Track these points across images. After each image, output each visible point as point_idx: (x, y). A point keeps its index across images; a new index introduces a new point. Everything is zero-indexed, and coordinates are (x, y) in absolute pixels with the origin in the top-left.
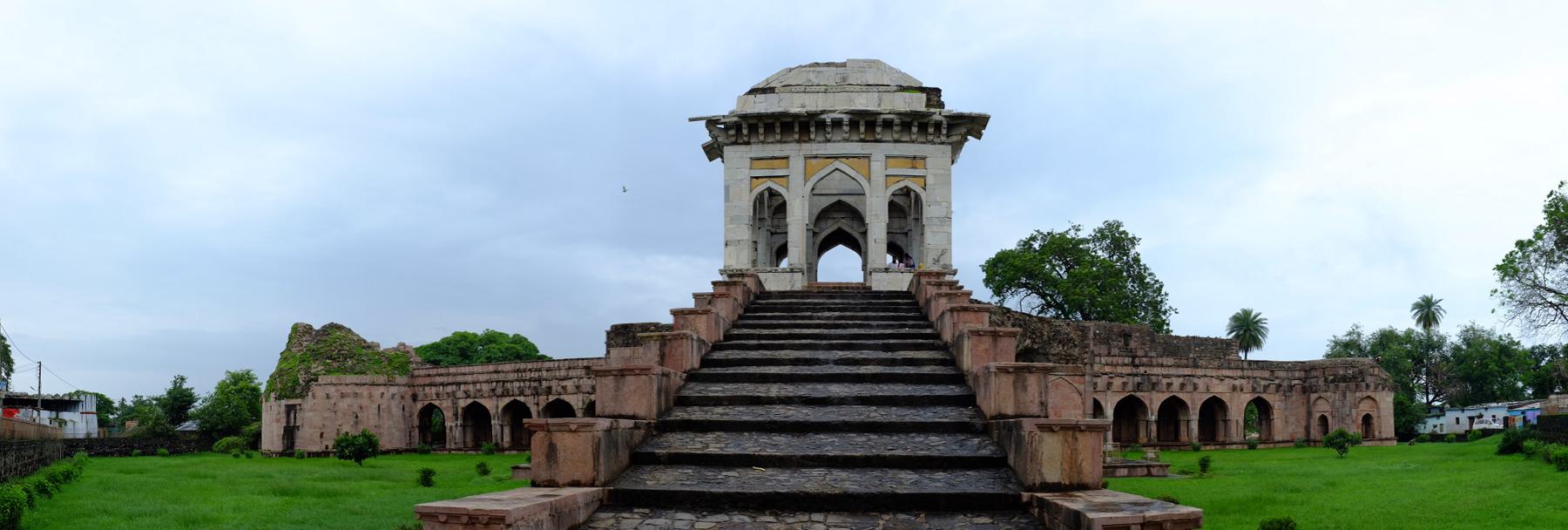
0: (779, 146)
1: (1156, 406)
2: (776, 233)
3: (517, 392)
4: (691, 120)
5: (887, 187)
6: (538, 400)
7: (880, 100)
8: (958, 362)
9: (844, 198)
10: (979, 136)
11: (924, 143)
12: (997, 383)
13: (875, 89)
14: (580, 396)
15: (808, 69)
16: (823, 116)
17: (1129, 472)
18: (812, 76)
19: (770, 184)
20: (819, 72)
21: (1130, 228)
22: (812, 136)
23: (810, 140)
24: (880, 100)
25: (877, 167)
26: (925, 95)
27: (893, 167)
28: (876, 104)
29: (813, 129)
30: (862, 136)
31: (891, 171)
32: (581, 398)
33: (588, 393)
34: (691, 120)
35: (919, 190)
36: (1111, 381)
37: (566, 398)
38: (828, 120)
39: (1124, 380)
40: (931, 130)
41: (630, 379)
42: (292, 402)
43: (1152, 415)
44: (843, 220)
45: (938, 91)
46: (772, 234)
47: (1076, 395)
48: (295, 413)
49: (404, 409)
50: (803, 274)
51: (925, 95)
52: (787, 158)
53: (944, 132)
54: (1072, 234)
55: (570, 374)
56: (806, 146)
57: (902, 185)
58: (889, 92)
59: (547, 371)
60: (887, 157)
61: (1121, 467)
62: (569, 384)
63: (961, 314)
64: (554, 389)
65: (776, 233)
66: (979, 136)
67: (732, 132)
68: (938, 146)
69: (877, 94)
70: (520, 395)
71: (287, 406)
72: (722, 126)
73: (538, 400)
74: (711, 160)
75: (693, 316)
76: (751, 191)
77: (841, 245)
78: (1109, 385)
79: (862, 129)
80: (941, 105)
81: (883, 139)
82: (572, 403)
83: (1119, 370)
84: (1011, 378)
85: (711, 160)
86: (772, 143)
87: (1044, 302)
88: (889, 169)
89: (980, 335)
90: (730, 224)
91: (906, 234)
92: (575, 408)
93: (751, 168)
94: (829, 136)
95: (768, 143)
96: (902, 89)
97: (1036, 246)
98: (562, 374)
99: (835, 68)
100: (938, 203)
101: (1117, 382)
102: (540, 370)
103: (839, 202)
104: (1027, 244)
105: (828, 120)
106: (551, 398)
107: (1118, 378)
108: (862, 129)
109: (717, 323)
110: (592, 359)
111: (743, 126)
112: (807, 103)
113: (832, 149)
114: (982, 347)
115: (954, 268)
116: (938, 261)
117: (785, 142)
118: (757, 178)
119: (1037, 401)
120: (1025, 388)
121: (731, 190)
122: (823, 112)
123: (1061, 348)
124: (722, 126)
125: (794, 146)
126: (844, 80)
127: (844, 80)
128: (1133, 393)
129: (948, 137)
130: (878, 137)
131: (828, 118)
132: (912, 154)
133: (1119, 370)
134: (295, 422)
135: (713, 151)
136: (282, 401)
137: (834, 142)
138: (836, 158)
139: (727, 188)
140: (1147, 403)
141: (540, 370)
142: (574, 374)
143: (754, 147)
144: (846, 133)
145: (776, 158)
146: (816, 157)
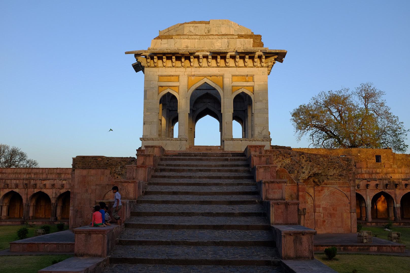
1: (399, 198)
2: (172, 110)
3: (13, 186)
4: (127, 53)
6: (27, 191)
9: (209, 92)
12: (285, 240)
13: (226, 37)
14: (54, 190)
17: (378, 249)
18: (192, 29)
20: (195, 27)
24: (229, 43)
26: (252, 40)
28: (226, 46)
32: (54, 192)
33: (59, 188)
34: (127, 53)
36: (369, 183)
37: (45, 191)
39: (377, 182)
41: (94, 236)
43: (397, 203)
44: (209, 104)
45: (259, 37)
46: (170, 111)
47: (345, 199)
51: (252, 40)
52: (178, 76)
55: (48, 177)
59: (35, 174)
60: (233, 76)
61: (373, 246)
62: (47, 183)
63: (270, 185)
64: (38, 186)
65: (172, 110)
70: (16, 188)
73: (27, 191)
74: (137, 71)
75: (126, 184)
76: (158, 94)
78: (367, 186)
80: (262, 45)
82: (49, 195)
84: (292, 238)
85: (137, 71)
88: (233, 83)
89: (278, 205)
90: (147, 112)
91: (244, 111)
92: (51, 197)
98: (43, 177)
99: (204, 25)
100: (261, 101)
101: (373, 184)
102: (30, 174)
103: (207, 93)
106: (36, 191)
107: (373, 181)
109: (139, 188)
110: (62, 168)
114: (280, 211)
116: (261, 133)
118: (162, 87)
119: (307, 250)
120: (301, 243)
121: (147, 93)
122: (198, 51)
123: (335, 172)
128: (383, 190)
131: (201, 54)
132: (246, 74)
135: (138, 67)
139: (145, 92)
140: (393, 196)
141: (30, 174)
142: (51, 177)
145: (172, 76)
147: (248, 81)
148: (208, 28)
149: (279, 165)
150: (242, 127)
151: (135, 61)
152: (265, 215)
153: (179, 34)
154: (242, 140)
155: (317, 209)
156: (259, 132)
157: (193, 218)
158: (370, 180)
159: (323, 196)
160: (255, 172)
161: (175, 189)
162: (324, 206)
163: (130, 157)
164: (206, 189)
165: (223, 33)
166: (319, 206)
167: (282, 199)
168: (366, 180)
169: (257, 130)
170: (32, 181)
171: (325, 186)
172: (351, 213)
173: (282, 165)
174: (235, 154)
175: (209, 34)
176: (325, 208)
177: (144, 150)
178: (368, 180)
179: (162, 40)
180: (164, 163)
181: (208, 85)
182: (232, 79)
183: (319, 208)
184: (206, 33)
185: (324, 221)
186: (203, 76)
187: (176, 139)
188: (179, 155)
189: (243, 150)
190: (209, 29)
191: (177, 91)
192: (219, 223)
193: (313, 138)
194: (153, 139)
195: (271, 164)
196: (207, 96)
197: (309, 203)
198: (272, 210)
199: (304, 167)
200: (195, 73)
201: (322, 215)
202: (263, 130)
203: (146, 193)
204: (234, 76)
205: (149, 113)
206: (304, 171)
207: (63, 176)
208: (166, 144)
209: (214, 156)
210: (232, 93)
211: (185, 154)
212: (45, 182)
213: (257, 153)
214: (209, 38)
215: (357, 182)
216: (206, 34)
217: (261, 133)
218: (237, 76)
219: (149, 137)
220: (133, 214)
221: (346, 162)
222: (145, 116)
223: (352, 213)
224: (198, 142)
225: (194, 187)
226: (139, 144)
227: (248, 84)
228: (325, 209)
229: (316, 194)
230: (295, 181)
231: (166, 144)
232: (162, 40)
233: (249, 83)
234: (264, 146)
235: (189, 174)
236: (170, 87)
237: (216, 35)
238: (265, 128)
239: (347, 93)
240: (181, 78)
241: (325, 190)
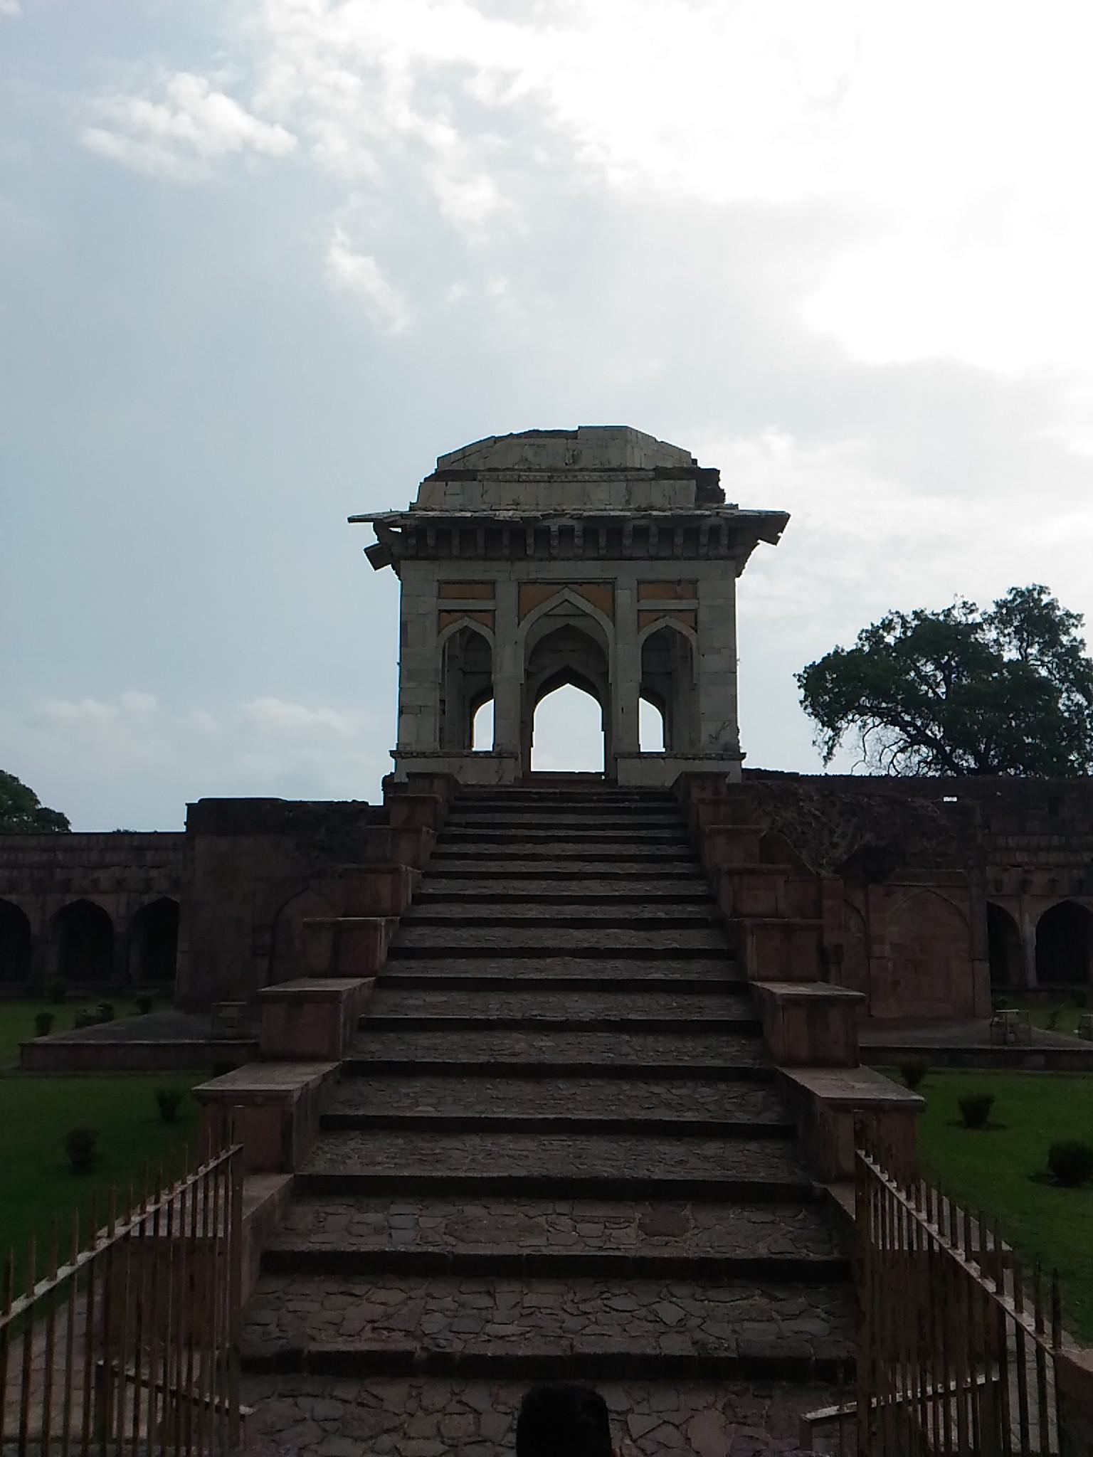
4: (351, 520)
5: (639, 629)
7: (630, 493)
9: (572, 622)
10: (774, 541)
11: (694, 559)
13: (621, 476)
15: (523, 441)
16: (546, 523)
18: (529, 453)
19: (466, 622)
21: (1065, 598)
23: (526, 557)
24: (630, 493)
25: (625, 597)
28: (623, 500)
29: (530, 541)
30: (602, 552)
34: (351, 520)
35: (687, 631)
37: (98, 900)
38: (554, 529)
40: (704, 540)
46: (465, 673)
50: (516, 759)
52: (493, 583)
53: (724, 541)
54: (958, 614)
57: (661, 624)
58: (642, 480)
60: (639, 582)
62: (104, 876)
66: (774, 541)
67: (413, 541)
68: (715, 562)
69: (624, 484)
72: (399, 530)
76: (439, 632)
77: (568, 685)
78: (1024, 885)
79: (602, 541)
81: (634, 555)
83: (1043, 857)
86: (471, 559)
87: (905, 736)
88: (642, 601)
94: (554, 552)
95: (466, 559)
96: (661, 474)
97: (890, 639)
101: (1039, 879)
104: (873, 635)
105: (554, 529)
106: (70, 899)
108: (602, 541)
111: (428, 534)
112: (522, 499)
113: (559, 570)
115: (742, 751)
116: (716, 738)
117: (491, 559)
118: (448, 611)
124: (399, 530)
126: (575, 459)
127: (575, 459)
129: (729, 548)
130: (627, 553)
131: (554, 525)
133: (1043, 857)
137: (562, 560)
138: (566, 584)
144: (579, 547)
145: (477, 582)
146: (534, 582)
147: (680, 598)
148: (574, 451)
149: (764, 826)
150: (664, 719)
151: (373, 540)
152: (732, 955)
153: (492, 467)
154: (664, 756)
155: (876, 949)
156: (710, 735)
158: (1033, 868)
160: (490, 957)
161: (497, 887)
163: (354, 801)
164: (574, 888)
165: (614, 465)
167: (776, 914)
168: (1020, 867)
169: (707, 730)
170: (59, 870)
172: (973, 960)
173: (773, 823)
174: (647, 794)
175: (577, 467)
177: (407, 784)
178: (1026, 868)
179: (447, 485)
180: (457, 818)
181: (666, 725)
182: (638, 590)
184: (566, 464)
186: (558, 583)
188: (499, 796)
189: (669, 783)
190: (575, 453)
191: (490, 625)
193: (864, 746)
194: (423, 755)
195: (78, 1291)
196: (568, 632)
198: (751, 942)
199: (837, 830)
201: (890, 965)
202: (723, 728)
203: (419, 899)
204: (644, 582)
206: (835, 839)
207: (149, 856)
208: (461, 767)
209: (592, 801)
210: (639, 629)
211: (511, 796)
212: (99, 874)
213: (708, 794)
214: (575, 479)
215: (991, 872)
216: (567, 467)
217: (716, 738)
218: (651, 582)
219: (414, 749)
220: (394, 953)
224: (541, 761)
225: (544, 884)
226: (389, 766)
227: (683, 605)
230: (811, 869)
231: (461, 767)
232: (447, 485)
233: (684, 601)
234: (726, 775)
235: (529, 848)
236: (470, 614)
237: (594, 470)
238: (727, 724)
239: (970, 619)
240: (500, 590)
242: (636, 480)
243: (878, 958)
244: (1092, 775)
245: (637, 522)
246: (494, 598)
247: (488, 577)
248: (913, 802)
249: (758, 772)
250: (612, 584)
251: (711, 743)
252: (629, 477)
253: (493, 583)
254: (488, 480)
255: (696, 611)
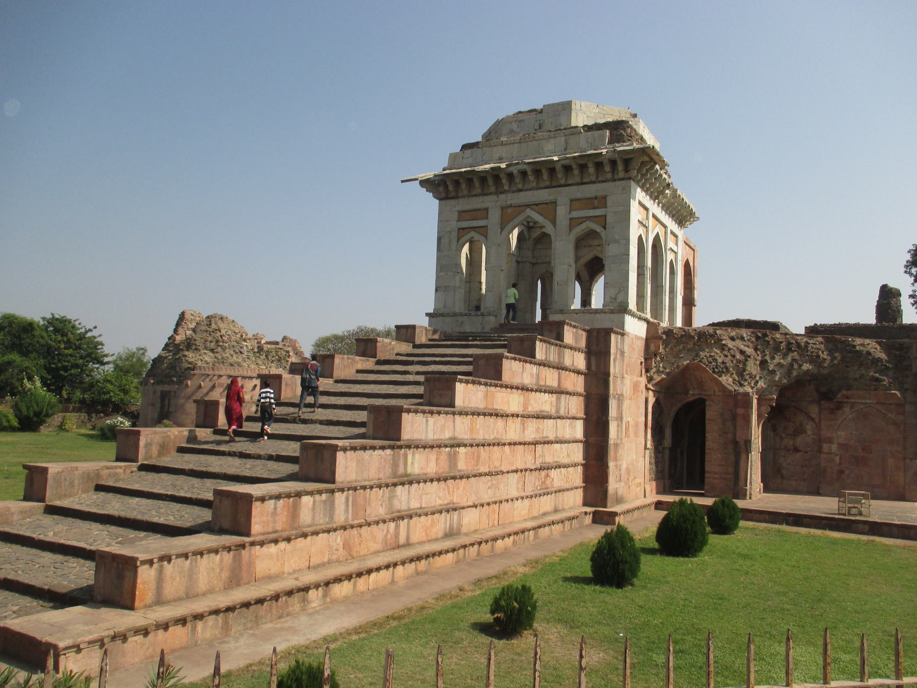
0: (480, 199)
4: (402, 182)
5: (570, 230)
8: (160, 425)
22: (506, 187)
25: (562, 211)
27: (578, 209)
31: (575, 214)
34: (402, 182)
38: (515, 172)
42: (166, 388)
48: (169, 400)
49: (745, 557)
52: (487, 210)
56: (502, 197)
60: (571, 201)
65: (537, 263)
71: (162, 392)
88: (572, 212)
93: (459, 220)
100: (617, 241)
116: (615, 299)
118: (463, 229)
125: (493, 198)
131: (515, 170)
134: (169, 407)
136: (224, 400)
143: (461, 200)
145: (479, 210)
146: (511, 206)
155: (825, 446)
156: (611, 297)
157: (324, 418)
159: (840, 420)
162: (841, 440)
166: (830, 441)
171: (846, 400)
176: (845, 444)
182: (570, 205)
183: (829, 445)
185: (841, 472)
187: (597, 311)
192: (331, 428)
197: (809, 432)
200: (512, 202)
201: (838, 458)
202: (619, 292)
205: (443, 274)
210: (570, 230)
218: (579, 200)
221: (897, 353)
222: (437, 277)
223: (908, 460)
227: (598, 212)
228: (842, 446)
229: (822, 416)
238: (622, 289)
241: (845, 409)
242: (571, 134)
243: (826, 453)
244: (913, 328)
245: (563, 162)
246: (487, 218)
247: (484, 206)
248: (853, 341)
249: (877, 318)
250: (554, 203)
251: (611, 302)
252: (566, 133)
253: (487, 210)
254: (485, 147)
255: (605, 216)
